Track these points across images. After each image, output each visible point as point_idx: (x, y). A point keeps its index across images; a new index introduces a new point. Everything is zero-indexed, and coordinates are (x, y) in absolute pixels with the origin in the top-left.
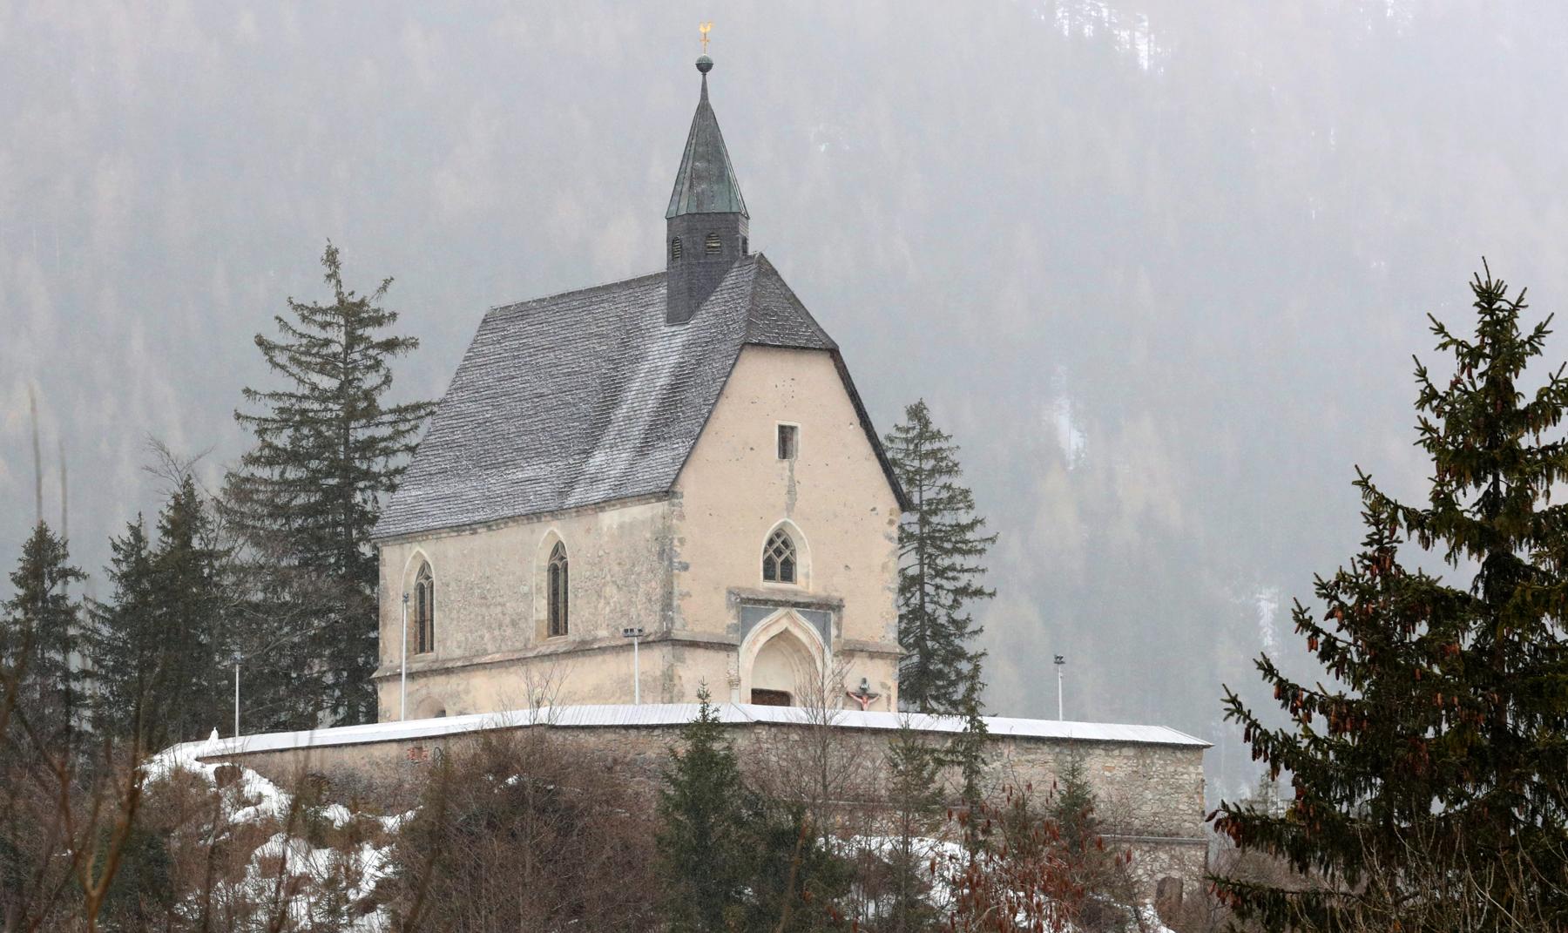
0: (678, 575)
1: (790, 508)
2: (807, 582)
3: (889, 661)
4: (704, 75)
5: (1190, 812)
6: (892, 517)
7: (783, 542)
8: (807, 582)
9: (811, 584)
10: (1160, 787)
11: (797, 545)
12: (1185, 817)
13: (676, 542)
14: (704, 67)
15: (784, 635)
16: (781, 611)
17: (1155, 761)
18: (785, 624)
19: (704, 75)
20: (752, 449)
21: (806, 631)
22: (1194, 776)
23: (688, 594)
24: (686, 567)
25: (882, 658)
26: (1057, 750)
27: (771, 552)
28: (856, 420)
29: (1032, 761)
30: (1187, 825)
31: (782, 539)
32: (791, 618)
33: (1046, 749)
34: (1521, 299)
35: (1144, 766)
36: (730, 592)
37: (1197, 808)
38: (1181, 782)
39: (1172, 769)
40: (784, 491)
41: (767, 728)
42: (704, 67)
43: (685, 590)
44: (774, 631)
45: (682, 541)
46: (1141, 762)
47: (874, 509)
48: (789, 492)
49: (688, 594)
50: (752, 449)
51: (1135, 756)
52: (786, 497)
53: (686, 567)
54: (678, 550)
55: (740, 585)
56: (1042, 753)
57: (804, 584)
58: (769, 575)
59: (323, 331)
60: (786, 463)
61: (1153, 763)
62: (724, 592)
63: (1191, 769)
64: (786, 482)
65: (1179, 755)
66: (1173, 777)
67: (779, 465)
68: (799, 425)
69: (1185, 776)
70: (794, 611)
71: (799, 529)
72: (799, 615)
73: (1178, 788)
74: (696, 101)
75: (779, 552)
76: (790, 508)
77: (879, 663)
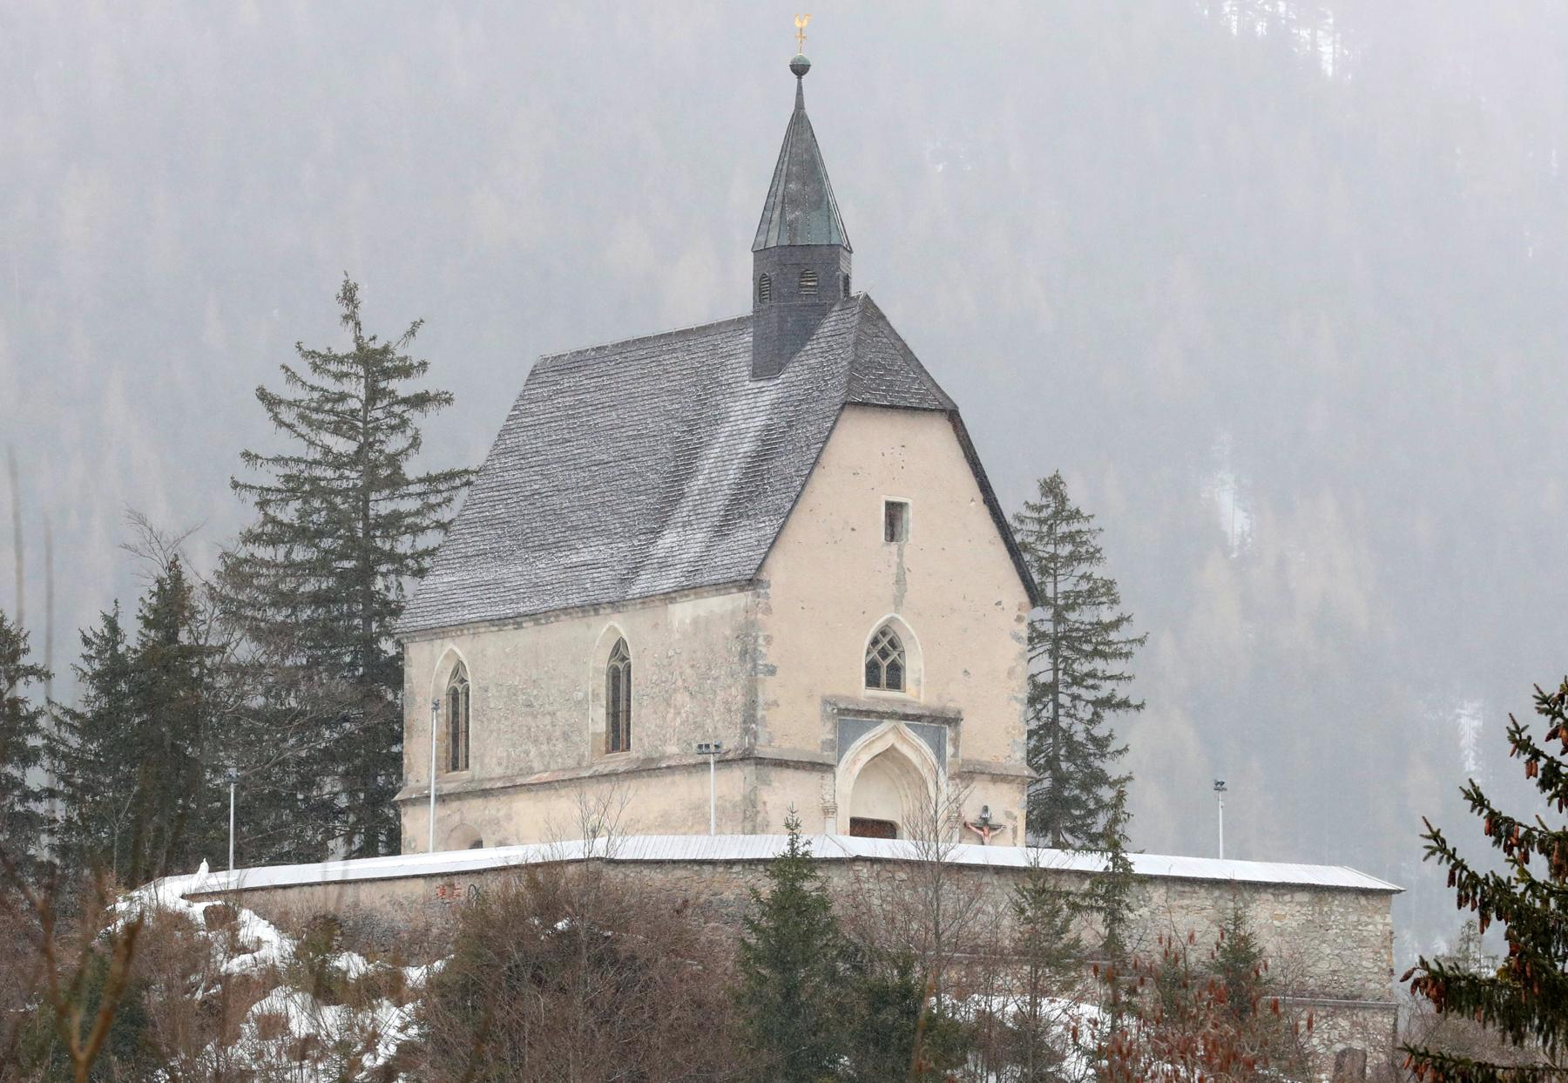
1: (898, 601)
2: (917, 691)
5: (1376, 970)
8: (917, 691)
9: (922, 692)
10: (1340, 940)
11: (906, 645)
12: (1370, 977)
13: (761, 641)
14: (800, 69)
16: (887, 724)
17: (1334, 908)
18: (891, 740)
20: (853, 529)
21: (917, 749)
22: (1380, 927)
23: (776, 704)
27: (875, 653)
31: (888, 638)
33: (1202, 892)
35: (1321, 914)
37: (1384, 965)
38: (1365, 934)
39: (1355, 919)
40: (892, 579)
42: (800, 69)
43: (771, 698)
44: (879, 748)
45: (768, 640)
47: (999, 603)
49: (776, 704)
50: (853, 529)
51: (1310, 903)
53: (772, 671)
54: (764, 650)
58: (873, 681)
60: (894, 546)
61: (1331, 910)
63: (1378, 918)
64: (894, 570)
65: (1363, 901)
66: (1355, 928)
67: (886, 549)
68: (910, 501)
69: (1370, 927)
70: (902, 725)
72: (908, 730)
73: (1362, 942)
75: (884, 654)
76: (898, 601)
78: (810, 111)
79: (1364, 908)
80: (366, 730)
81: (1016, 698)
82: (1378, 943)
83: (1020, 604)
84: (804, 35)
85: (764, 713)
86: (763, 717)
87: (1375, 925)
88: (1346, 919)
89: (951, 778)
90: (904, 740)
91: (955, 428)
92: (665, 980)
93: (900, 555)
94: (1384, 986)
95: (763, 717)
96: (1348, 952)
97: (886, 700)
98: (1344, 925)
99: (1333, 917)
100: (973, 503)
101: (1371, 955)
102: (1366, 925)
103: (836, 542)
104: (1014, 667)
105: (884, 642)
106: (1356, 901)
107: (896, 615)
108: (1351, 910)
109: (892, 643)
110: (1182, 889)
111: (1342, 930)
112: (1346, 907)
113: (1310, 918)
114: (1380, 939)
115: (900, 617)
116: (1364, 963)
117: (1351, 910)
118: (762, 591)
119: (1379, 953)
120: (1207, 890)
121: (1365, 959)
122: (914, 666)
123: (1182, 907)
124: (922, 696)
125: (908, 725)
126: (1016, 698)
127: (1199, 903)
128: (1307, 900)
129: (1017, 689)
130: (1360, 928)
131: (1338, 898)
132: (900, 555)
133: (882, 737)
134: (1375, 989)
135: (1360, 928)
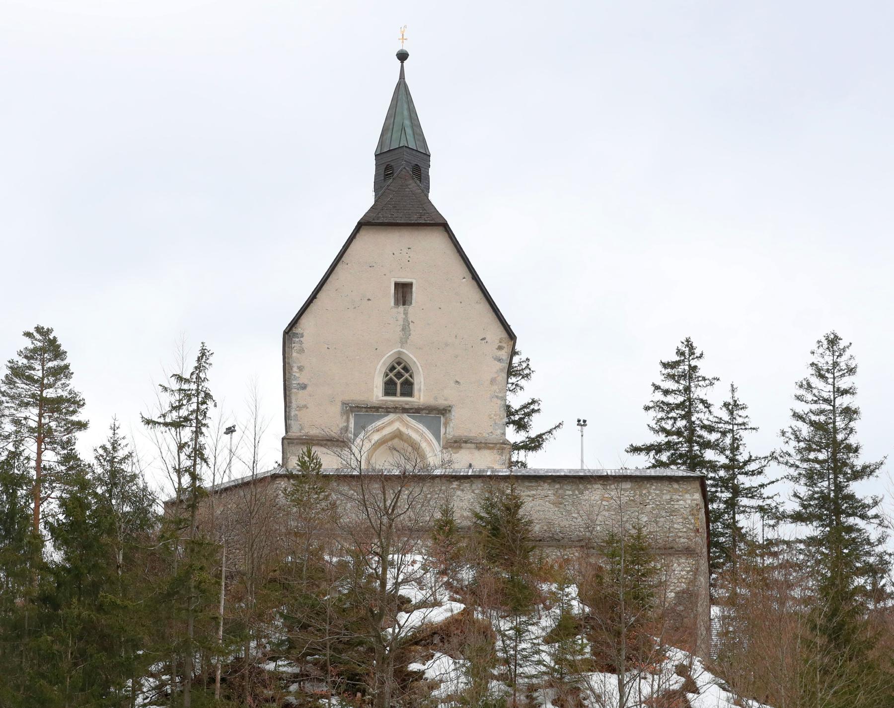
0: (296, 393)
2: (421, 396)
3: (495, 451)
4: (402, 62)
5: (685, 530)
6: (501, 344)
7: (399, 365)
8: (421, 396)
9: (422, 395)
11: (413, 369)
12: (680, 534)
13: (295, 369)
14: (403, 56)
15: (398, 435)
16: (392, 416)
17: (652, 491)
18: (397, 425)
19: (402, 62)
20: (369, 300)
21: (417, 431)
22: (689, 502)
23: (305, 407)
24: (304, 387)
25: (489, 448)
26: (557, 486)
27: (391, 375)
28: (469, 276)
29: (533, 496)
30: (682, 540)
31: (396, 365)
32: (402, 421)
33: (546, 486)
34: (403, 42)
35: (641, 495)
36: (343, 403)
37: (691, 527)
38: (676, 507)
39: (668, 497)
40: (399, 329)
41: (286, 479)
42: (403, 56)
43: (302, 403)
44: (387, 431)
45: (301, 369)
46: (638, 492)
47: (484, 339)
48: (403, 330)
49: (305, 407)
50: (369, 300)
51: (631, 489)
52: (401, 333)
53: (304, 387)
54: (297, 375)
55: (354, 399)
56: (542, 490)
57: (418, 397)
58: (387, 393)
59: (665, 397)
60: (401, 308)
61: (649, 492)
62: (340, 404)
63: (687, 496)
64: (401, 322)
65: (676, 486)
66: (668, 503)
68: (414, 281)
69: (681, 502)
70: (405, 416)
71: (411, 356)
72: (409, 419)
73: (673, 512)
74: (397, 79)
75: (399, 375)
76: (403, 342)
77: (486, 453)
78: (408, 80)
79: (676, 491)
80: (803, 603)
81: (497, 397)
82: (686, 513)
83: (501, 339)
84: (404, 38)
85: (296, 412)
86: (296, 415)
87: (685, 501)
88: (661, 498)
89: (445, 447)
90: (408, 426)
91: (449, 234)
92: (801, 679)
93: (406, 314)
94: (691, 540)
95: (296, 415)
96: (662, 519)
97: (399, 401)
98: (660, 502)
99: (650, 498)
100: (464, 280)
101: (681, 520)
102: (678, 501)
103: (355, 308)
104: (495, 378)
105: (399, 368)
106: (670, 486)
107: (401, 350)
108: (665, 492)
109: (406, 369)
110: (530, 485)
111: (658, 505)
112: (661, 491)
113: (632, 498)
114: (688, 510)
115: (404, 351)
116: (675, 526)
117: (665, 492)
118: (297, 340)
119: (687, 518)
120: (549, 484)
121: (675, 523)
122: (420, 382)
123: (529, 496)
124: (422, 398)
125: (408, 416)
126: (497, 397)
127: (543, 493)
128: (629, 487)
129: (498, 391)
130: (672, 503)
131: (655, 484)
132: (406, 314)
133: (391, 424)
134: (684, 543)
135: (672, 503)
